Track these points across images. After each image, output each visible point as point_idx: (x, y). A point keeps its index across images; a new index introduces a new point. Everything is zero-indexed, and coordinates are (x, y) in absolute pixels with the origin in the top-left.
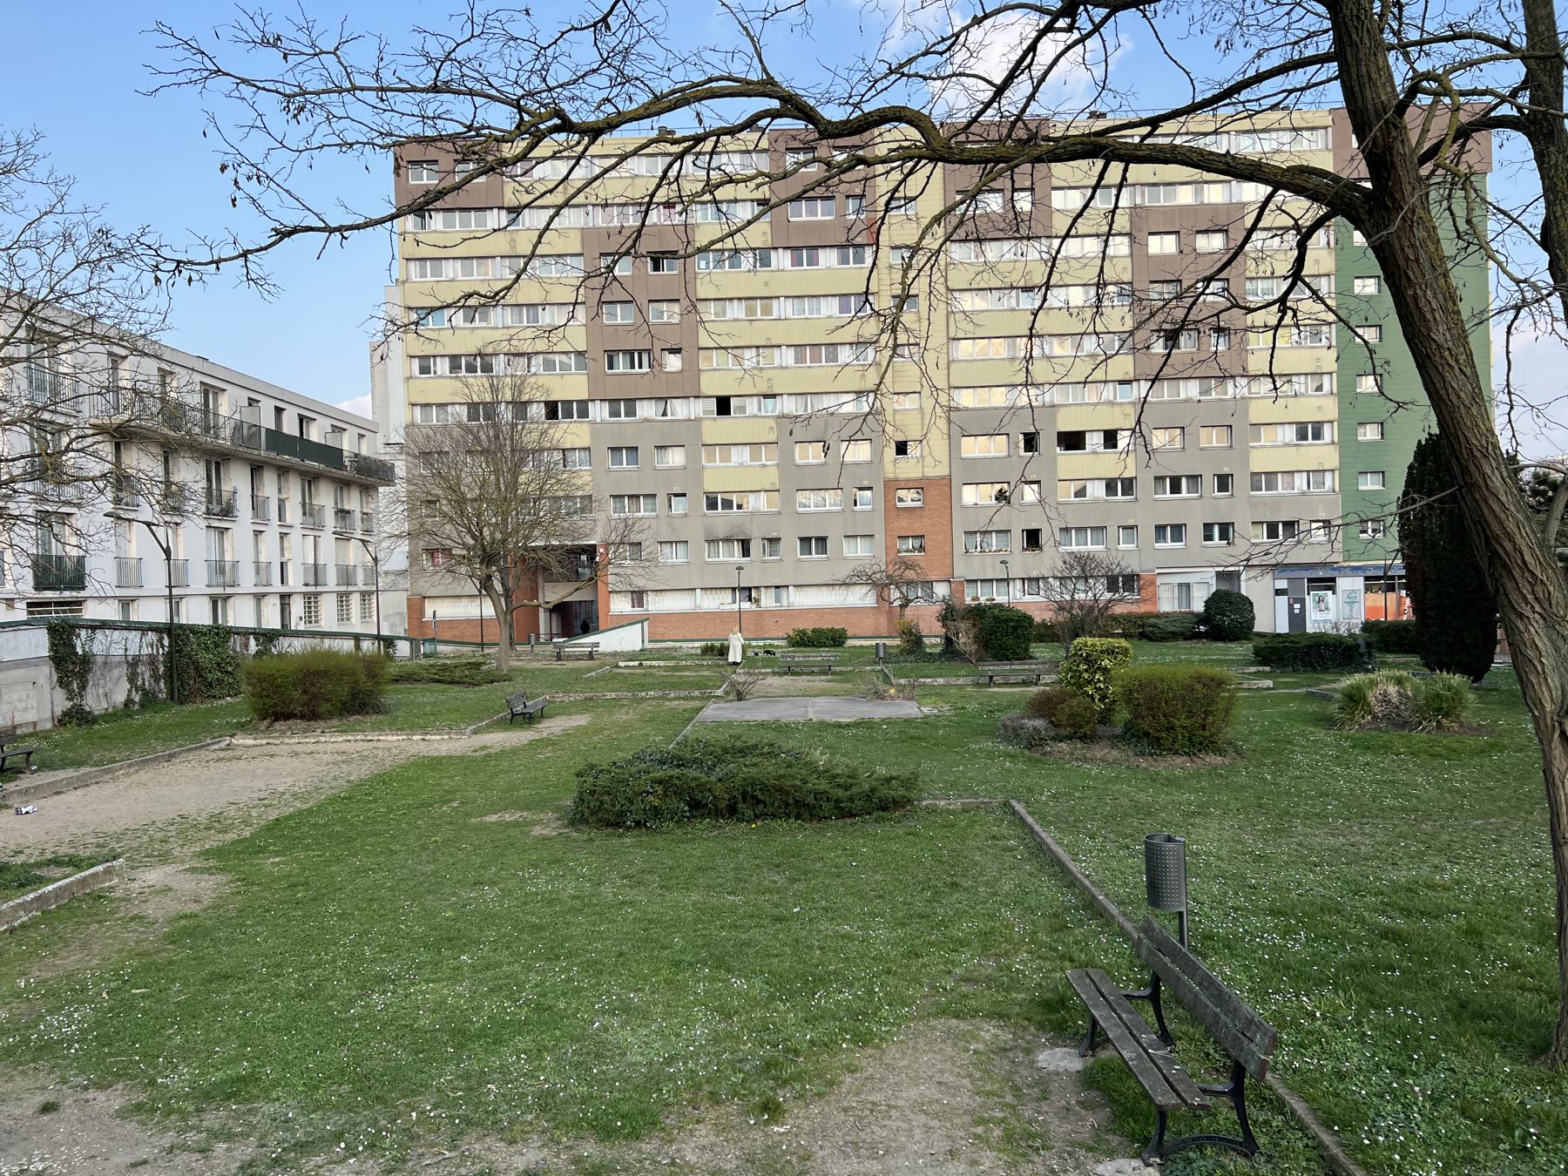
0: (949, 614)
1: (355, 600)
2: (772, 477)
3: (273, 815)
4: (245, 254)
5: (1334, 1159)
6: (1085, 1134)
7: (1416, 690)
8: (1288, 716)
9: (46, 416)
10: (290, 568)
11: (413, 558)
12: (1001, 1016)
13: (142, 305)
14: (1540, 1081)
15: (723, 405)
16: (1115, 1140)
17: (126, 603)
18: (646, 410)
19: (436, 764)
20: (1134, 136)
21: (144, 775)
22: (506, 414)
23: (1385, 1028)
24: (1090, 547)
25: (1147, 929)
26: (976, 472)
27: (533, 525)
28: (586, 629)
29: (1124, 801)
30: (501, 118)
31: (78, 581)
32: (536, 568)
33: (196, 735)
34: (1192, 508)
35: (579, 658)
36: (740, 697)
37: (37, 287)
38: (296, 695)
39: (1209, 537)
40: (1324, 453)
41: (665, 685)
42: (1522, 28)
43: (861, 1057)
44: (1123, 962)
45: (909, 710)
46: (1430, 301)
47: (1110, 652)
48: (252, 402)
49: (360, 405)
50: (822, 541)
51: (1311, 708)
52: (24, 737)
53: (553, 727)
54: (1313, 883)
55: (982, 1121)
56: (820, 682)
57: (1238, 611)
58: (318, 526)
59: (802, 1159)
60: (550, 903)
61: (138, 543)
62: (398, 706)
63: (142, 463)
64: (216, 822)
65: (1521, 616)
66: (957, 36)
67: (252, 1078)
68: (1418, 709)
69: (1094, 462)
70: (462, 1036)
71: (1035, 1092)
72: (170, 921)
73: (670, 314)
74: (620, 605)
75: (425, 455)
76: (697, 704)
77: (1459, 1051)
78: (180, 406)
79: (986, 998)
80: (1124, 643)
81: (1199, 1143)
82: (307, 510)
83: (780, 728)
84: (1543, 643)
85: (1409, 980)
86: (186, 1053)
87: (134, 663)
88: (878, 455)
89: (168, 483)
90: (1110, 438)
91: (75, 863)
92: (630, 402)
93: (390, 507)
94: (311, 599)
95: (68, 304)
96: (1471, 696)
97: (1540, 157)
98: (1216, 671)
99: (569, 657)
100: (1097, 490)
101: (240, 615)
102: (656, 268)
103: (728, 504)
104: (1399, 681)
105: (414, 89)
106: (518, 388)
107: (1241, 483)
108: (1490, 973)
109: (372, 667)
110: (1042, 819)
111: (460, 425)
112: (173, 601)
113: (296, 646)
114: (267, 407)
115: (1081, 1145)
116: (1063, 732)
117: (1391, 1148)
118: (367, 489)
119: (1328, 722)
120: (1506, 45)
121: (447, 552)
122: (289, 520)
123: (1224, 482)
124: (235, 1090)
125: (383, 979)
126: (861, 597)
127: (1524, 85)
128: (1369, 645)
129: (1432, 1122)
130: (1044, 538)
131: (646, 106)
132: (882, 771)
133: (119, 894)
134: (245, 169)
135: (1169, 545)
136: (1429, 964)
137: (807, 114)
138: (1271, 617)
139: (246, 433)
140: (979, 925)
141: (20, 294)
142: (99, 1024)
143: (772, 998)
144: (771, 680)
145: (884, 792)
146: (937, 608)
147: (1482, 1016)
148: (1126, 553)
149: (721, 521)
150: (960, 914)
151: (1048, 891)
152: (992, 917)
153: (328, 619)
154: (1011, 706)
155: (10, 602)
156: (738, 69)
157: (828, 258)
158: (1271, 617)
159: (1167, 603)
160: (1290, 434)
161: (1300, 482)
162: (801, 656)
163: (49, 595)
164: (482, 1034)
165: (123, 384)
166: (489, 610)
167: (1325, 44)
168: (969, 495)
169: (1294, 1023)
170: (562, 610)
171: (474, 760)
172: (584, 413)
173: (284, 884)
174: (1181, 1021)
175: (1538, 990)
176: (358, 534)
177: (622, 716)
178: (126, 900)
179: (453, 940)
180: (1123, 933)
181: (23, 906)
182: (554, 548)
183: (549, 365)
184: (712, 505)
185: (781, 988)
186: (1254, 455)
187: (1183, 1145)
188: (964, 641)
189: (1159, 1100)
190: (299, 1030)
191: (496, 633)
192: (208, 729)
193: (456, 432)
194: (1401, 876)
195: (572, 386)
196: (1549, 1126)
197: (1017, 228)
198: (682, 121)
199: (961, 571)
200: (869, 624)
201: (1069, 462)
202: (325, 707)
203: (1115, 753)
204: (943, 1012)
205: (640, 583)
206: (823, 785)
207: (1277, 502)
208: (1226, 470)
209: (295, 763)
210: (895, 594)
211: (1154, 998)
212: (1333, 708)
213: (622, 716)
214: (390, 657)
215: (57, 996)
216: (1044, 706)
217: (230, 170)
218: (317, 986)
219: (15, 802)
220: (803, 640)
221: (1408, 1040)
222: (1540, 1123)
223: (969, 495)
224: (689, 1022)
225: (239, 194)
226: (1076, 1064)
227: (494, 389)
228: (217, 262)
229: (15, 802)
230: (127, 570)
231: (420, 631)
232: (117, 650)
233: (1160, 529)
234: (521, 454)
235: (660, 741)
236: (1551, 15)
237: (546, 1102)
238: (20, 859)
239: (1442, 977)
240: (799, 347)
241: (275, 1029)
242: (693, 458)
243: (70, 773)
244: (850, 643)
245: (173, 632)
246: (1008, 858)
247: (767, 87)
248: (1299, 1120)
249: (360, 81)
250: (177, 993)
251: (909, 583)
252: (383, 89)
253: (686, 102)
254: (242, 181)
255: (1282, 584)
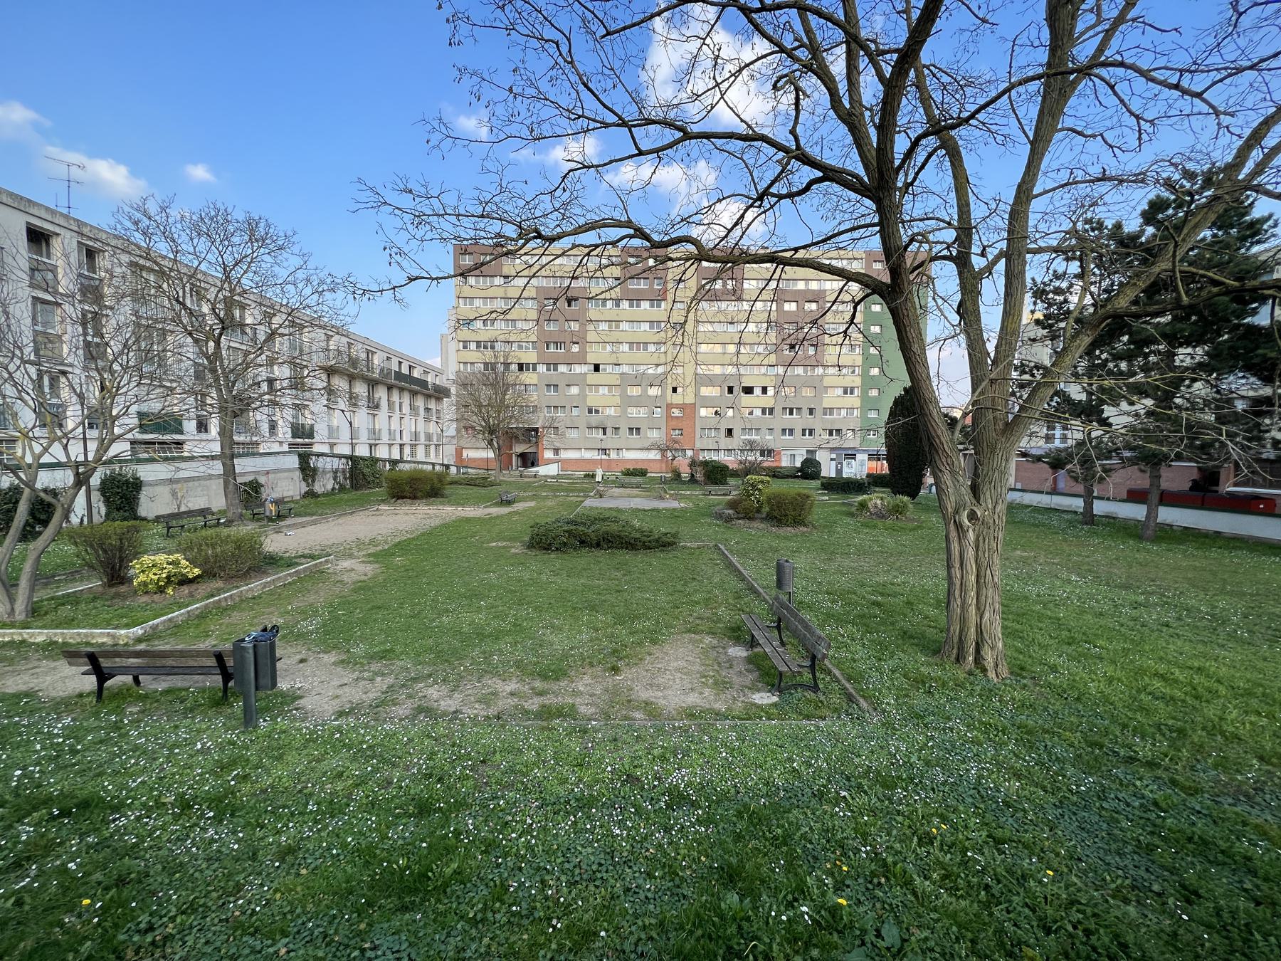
0: (693, 464)
1: (432, 448)
2: (617, 400)
3: (397, 540)
4: (394, 288)
5: (850, 694)
6: (748, 683)
7: (889, 503)
8: (834, 512)
9: (298, 361)
10: (404, 432)
11: (458, 430)
12: (713, 634)
13: (342, 312)
14: (937, 665)
15: (597, 368)
16: (760, 685)
17: (332, 445)
18: (563, 368)
19: (468, 520)
20: (788, 254)
21: (340, 521)
22: (501, 368)
23: (873, 641)
24: (754, 437)
25: (777, 599)
26: (707, 402)
27: (511, 418)
28: (533, 465)
29: (765, 545)
30: (511, 231)
31: (311, 436)
32: (512, 436)
33: (363, 504)
34: (796, 421)
35: (530, 477)
36: (601, 496)
37: (294, 302)
38: (407, 488)
39: (804, 435)
40: (854, 401)
41: (568, 490)
42: (956, 217)
43: (653, 649)
44: (765, 612)
45: (675, 504)
46: (911, 333)
47: (762, 482)
48: (388, 358)
49: (436, 362)
50: (638, 429)
51: (844, 509)
52: (288, 502)
53: (519, 506)
54: (844, 582)
55: (705, 677)
56: (635, 492)
57: (815, 467)
58: (417, 414)
59: (628, 690)
60: (519, 581)
61: (338, 419)
62: (452, 494)
63: (340, 383)
64: (373, 542)
65: (941, 471)
66: (711, 206)
67: (391, 651)
68: (889, 511)
69: (757, 400)
70: (482, 636)
71: (727, 665)
72: (354, 583)
73: (575, 326)
74: (548, 455)
75: (465, 385)
76: (582, 499)
77: (903, 652)
78: (357, 359)
79: (705, 626)
80: (768, 478)
81: (795, 687)
82: (412, 407)
83: (618, 510)
84: (949, 483)
85: (883, 622)
86: (363, 639)
87: (336, 472)
88: (664, 392)
89: (351, 393)
90: (764, 390)
91: (312, 557)
92: (556, 365)
93: (448, 407)
94: (413, 447)
95: (308, 312)
96: (911, 506)
97: (960, 274)
98: (806, 491)
99: (526, 477)
100: (758, 412)
101: (382, 453)
102: (569, 306)
103: (597, 412)
104: (882, 499)
105: (473, 216)
106: (506, 357)
107: (818, 412)
108: (917, 619)
109: (441, 478)
110: (732, 552)
111: (480, 372)
112: (353, 446)
113: (407, 467)
114: (395, 361)
115: (746, 687)
116: (741, 516)
117: (875, 690)
118: (439, 399)
119: (852, 515)
120: (949, 223)
121: (473, 428)
122: (404, 412)
123: (811, 411)
124: (384, 655)
125: (447, 611)
126: (654, 455)
127: (956, 240)
128: (869, 483)
129: (892, 679)
130: (734, 432)
131: (575, 229)
132: (663, 530)
133: (331, 571)
134: (395, 250)
135: (788, 437)
136: (891, 616)
137: (646, 237)
138: (828, 470)
139: (385, 373)
140: (704, 595)
141: (286, 305)
142: (324, 626)
143: (615, 624)
144: (614, 490)
145: (664, 539)
146: (688, 461)
147: (912, 637)
148: (769, 440)
149: (594, 419)
150: (696, 591)
151: (733, 582)
152: (709, 592)
153: (420, 455)
154: (718, 504)
155: (281, 443)
156: (616, 215)
157: (645, 305)
158: (828, 470)
159: (785, 463)
160: (840, 392)
161: (844, 412)
162: (628, 480)
163: (299, 440)
164: (490, 635)
165: (331, 347)
166: (491, 455)
167: (876, 220)
168: (703, 412)
169: (836, 639)
170: (523, 456)
171: (484, 519)
172: (534, 369)
173: (403, 569)
174: (789, 637)
175: (936, 627)
176: (434, 419)
177: (549, 503)
178: (335, 573)
179: (475, 595)
180: (765, 600)
181: (289, 575)
182: (521, 428)
183: (520, 347)
184: (590, 411)
185: (619, 619)
186: (825, 400)
187: (789, 688)
188: (699, 476)
189: (780, 669)
190: (411, 631)
191: (494, 465)
192: (369, 502)
193: (479, 375)
194: (881, 579)
195: (530, 357)
196: (940, 683)
197: (737, 295)
198: (590, 238)
199: (698, 445)
200: (656, 467)
201: (746, 399)
202: (419, 494)
203: (763, 525)
204: (689, 631)
205: (558, 445)
206: (638, 535)
207: (834, 421)
208: (812, 406)
209: (407, 518)
210: (669, 454)
211: (778, 627)
212: (854, 509)
213: (549, 503)
214: (448, 474)
215: (305, 614)
216: (733, 505)
217: (388, 250)
218: (419, 613)
219: (284, 530)
220: (628, 473)
221: (883, 646)
222: (936, 682)
223: (703, 412)
224: (580, 633)
225: (393, 261)
226: (745, 654)
227: (496, 357)
228: (381, 291)
229: (284, 530)
230: (332, 431)
231: (461, 463)
232: (328, 466)
233: (784, 430)
234: (507, 387)
235: (566, 514)
236: (969, 211)
237: (518, 665)
238: (287, 555)
239: (897, 621)
240: (631, 343)
241: (401, 630)
242: (582, 390)
243: (308, 518)
244: (649, 475)
245: (352, 458)
246: (716, 567)
247: (629, 224)
248: (837, 678)
249: (449, 211)
250: (358, 614)
251: (675, 450)
252: (459, 215)
253: (594, 228)
254: (393, 255)
255: (834, 456)
